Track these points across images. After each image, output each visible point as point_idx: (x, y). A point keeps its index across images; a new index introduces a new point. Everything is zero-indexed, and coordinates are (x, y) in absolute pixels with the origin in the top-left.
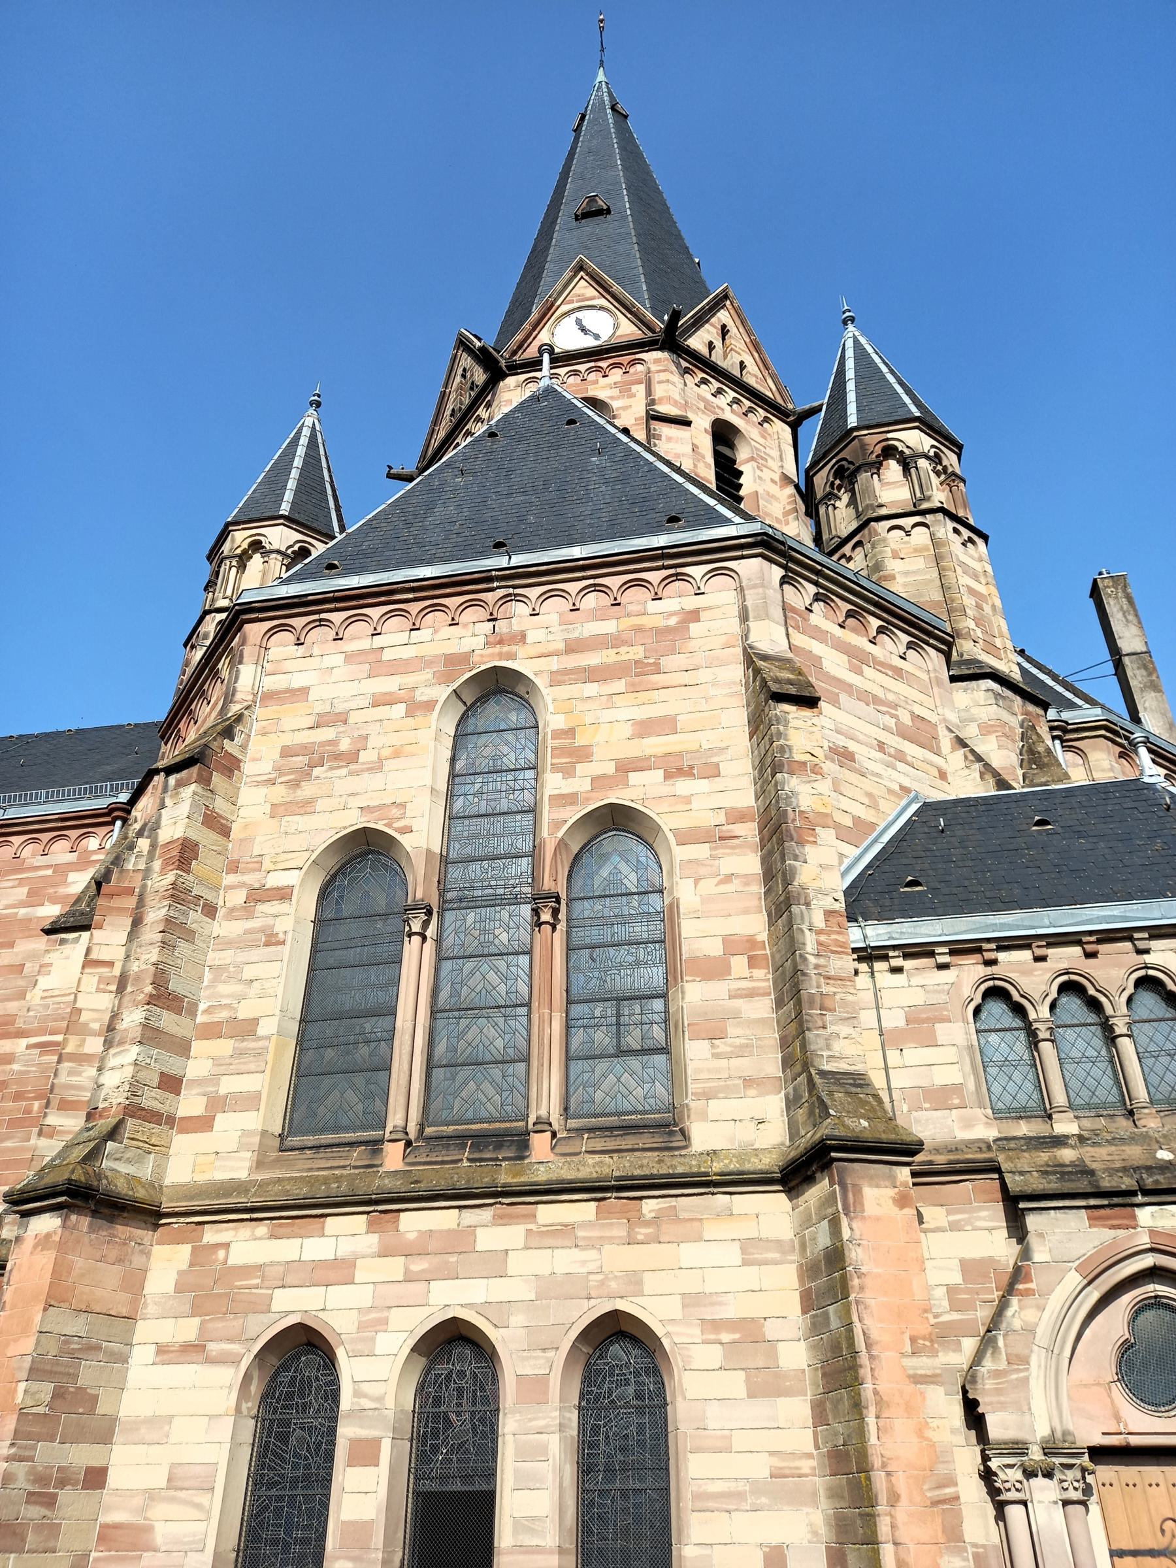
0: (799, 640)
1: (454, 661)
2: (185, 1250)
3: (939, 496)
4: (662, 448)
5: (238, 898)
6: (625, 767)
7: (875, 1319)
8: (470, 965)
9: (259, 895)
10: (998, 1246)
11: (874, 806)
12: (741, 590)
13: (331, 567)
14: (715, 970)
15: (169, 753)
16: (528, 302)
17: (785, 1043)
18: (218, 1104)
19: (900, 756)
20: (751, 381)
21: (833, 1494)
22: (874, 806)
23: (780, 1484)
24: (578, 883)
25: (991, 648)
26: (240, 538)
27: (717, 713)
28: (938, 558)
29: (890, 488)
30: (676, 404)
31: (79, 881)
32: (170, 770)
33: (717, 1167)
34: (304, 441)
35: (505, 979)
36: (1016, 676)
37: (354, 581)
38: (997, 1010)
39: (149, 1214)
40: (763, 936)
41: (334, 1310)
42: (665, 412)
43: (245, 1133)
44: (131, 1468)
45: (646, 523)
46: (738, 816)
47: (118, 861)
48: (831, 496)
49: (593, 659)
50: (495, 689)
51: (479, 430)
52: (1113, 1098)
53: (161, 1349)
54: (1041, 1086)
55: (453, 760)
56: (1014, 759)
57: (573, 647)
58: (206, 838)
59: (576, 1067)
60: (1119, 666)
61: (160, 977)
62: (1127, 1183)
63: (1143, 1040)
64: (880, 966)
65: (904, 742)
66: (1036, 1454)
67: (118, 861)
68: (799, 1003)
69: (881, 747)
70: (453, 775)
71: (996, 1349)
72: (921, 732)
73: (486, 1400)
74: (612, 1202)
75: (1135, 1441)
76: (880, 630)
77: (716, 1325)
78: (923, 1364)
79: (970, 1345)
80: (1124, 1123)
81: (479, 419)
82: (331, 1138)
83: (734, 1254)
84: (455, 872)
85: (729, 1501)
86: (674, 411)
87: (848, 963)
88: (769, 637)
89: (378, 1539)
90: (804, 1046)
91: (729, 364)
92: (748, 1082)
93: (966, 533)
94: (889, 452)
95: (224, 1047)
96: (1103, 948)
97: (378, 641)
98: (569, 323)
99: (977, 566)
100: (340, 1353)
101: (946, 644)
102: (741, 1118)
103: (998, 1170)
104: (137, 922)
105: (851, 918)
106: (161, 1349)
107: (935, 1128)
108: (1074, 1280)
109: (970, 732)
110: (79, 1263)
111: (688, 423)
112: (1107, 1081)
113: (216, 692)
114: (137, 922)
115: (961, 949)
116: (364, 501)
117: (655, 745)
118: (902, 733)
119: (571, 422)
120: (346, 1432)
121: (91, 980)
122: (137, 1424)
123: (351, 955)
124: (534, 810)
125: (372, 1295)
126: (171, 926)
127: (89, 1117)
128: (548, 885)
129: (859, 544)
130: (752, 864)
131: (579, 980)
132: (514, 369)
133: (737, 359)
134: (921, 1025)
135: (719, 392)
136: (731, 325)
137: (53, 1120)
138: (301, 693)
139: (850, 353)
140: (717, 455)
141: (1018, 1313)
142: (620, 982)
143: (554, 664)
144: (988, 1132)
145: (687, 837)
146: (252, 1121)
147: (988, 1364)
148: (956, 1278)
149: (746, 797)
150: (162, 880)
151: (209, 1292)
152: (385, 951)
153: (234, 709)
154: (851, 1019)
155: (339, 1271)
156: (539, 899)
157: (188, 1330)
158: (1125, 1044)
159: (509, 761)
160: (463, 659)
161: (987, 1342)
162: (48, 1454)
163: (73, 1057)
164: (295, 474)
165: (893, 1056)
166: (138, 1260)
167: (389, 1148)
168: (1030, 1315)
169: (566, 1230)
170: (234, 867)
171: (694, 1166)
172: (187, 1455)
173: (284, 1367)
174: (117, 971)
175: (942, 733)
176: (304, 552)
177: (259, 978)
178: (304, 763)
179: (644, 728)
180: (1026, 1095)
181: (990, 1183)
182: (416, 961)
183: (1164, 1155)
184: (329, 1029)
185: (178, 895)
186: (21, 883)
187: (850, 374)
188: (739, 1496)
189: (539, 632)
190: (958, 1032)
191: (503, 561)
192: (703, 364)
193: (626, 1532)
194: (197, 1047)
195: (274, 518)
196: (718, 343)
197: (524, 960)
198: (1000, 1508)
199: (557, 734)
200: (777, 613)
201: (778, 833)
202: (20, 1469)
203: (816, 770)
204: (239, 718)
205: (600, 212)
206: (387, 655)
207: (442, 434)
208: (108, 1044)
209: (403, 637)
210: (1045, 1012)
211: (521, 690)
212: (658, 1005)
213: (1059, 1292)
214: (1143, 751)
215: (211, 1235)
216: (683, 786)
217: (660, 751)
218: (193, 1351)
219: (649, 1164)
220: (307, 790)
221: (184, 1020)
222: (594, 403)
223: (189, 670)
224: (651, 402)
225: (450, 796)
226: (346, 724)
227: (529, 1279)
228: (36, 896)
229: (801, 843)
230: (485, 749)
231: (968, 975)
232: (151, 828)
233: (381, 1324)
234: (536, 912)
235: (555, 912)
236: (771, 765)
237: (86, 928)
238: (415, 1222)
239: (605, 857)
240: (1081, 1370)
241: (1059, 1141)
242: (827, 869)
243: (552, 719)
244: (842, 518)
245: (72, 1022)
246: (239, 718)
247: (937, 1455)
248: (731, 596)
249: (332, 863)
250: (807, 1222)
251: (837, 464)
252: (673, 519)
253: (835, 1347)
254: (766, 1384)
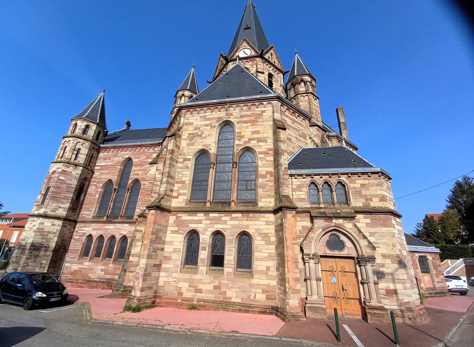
0: (283, 117)
1: (220, 118)
2: (175, 217)
3: (311, 90)
4: (259, 78)
5: (181, 160)
6: (250, 140)
7: (288, 234)
8: (221, 174)
9: (185, 160)
10: (309, 224)
11: (294, 149)
12: (273, 107)
13: (197, 99)
14: (264, 177)
15: (169, 134)
16: (234, 47)
17: (275, 190)
18: (179, 194)
19: (300, 140)
20: (276, 65)
21: (278, 259)
22: (294, 149)
23: (269, 257)
24: (240, 160)
25: (317, 120)
26: (180, 93)
27: (267, 130)
28: (309, 102)
29: (302, 88)
30: (262, 69)
31: (155, 156)
32: (169, 137)
33: (262, 209)
34: (191, 74)
35: (227, 176)
36: (321, 126)
37: (201, 102)
38: (313, 186)
39: (169, 211)
40: (273, 171)
41: (199, 227)
42: (259, 70)
43: (184, 199)
44: (168, 248)
45: (254, 93)
46: (270, 150)
47: (161, 152)
48: (290, 89)
49: (245, 119)
50: (227, 124)
51: (224, 73)
52: (331, 201)
53: (172, 231)
54: (319, 199)
55: (219, 137)
56: (320, 141)
57: (241, 117)
58: (176, 149)
59: (239, 192)
60: (339, 125)
61: (169, 173)
62: (332, 215)
63: (337, 192)
64: (293, 177)
65: (301, 137)
66: (311, 256)
67: (161, 152)
68: (279, 184)
69: (296, 138)
70: (219, 140)
71: (306, 240)
72: (304, 136)
73: (223, 242)
74: (245, 214)
75: (327, 255)
76: (298, 116)
77: (261, 234)
78: (295, 242)
79: (302, 239)
80: (332, 206)
81: (224, 71)
82: (198, 201)
83: (264, 223)
84: (219, 157)
85: (261, 259)
86: (261, 71)
87: (288, 176)
88: (277, 116)
89: (206, 261)
90: (279, 191)
91: (272, 61)
92: (269, 196)
93: (315, 98)
94: (302, 81)
95: (180, 185)
96: (332, 176)
97: (206, 114)
98: (242, 51)
99: (316, 104)
100: (200, 234)
101: (310, 120)
102: (267, 202)
103: (310, 212)
104: (165, 163)
105: (289, 169)
106: (172, 231)
107: (299, 205)
108: (321, 230)
109: (312, 136)
110: (158, 218)
111: (264, 73)
112: (330, 199)
113: (177, 123)
114: (165, 163)
115: (308, 175)
116: (203, 88)
117: (255, 136)
118: (300, 135)
119: (242, 72)
120: (201, 245)
121: (157, 173)
122: (168, 242)
123: (201, 171)
124: (233, 147)
125: (205, 226)
126: (170, 164)
127: (159, 195)
128: (235, 160)
129: (295, 99)
130: (271, 158)
131: (240, 177)
132: (231, 61)
133: (274, 60)
134: (299, 188)
135: (270, 67)
136: (273, 53)
137: (152, 195)
138: (192, 124)
139: (296, 60)
140: (269, 80)
141: (311, 235)
142: (247, 178)
143: (238, 120)
144: (308, 206)
145: (260, 153)
146: (185, 197)
147: (305, 242)
148: (301, 229)
149: (271, 146)
150: (169, 156)
151: (179, 223)
152: (207, 171)
153: (180, 126)
154: (287, 186)
155: (200, 222)
156: (233, 163)
157: (176, 229)
158: (334, 193)
159: (229, 137)
160: (220, 118)
161: (305, 239)
162: (155, 245)
163: (155, 185)
164: (190, 81)
165: (294, 193)
166: (167, 218)
167: (207, 203)
168: (313, 235)
169: (237, 218)
170: (180, 155)
171: (258, 209)
172: (175, 247)
173: (191, 235)
174: (162, 171)
175: (307, 136)
176: (192, 97)
177: (186, 174)
178: (192, 137)
179: (254, 133)
180: (315, 199)
181: (309, 214)
182: (212, 172)
183: (338, 211)
184: (197, 183)
185: (171, 159)
186: (145, 155)
187: (296, 64)
188: (263, 259)
189: (235, 113)
190: (306, 189)
191: (229, 100)
192: (267, 61)
193: (244, 262)
194: (175, 185)
195: (186, 90)
196: (270, 57)
197: (231, 173)
198: (304, 263)
199: (238, 133)
200: (279, 111)
201: (277, 153)
202: (151, 247)
203: (285, 142)
204: (181, 128)
205: (249, 28)
206: (207, 117)
207: (217, 74)
208: (161, 184)
209: (210, 113)
210: (321, 187)
211: (231, 124)
212: (254, 182)
213: (318, 232)
214: (343, 141)
215: (179, 215)
216: (260, 144)
217: (256, 137)
218: (176, 232)
219: (251, 208)
220: (193, 141)
221: (173, 180)
222: (246, 68)
223: (172, 118)
224: (257, 69)
225: (218, 143)
226: (200, 129)
227: (230, 225)
228: (147, 158)
229: (281, 155)
230: (225, 135)
231: (309, 180)
232: (166, 147)
233: (207, 230)
234: (233, 165)
235: (236, 165)
236: (277, 140)
237: (156, 164)
238: (211, 215)
239: (245, 156)
240: (320, 244)
241: (321, 208)
242: (285, 160)
243: (237, 130)
244: (292, 94)
245: (155, 179)
246: (181, 128)
247: (296, 255)
248: (271, 108)
249: (198, 154)
250: (277, 219)
251: (292, 83)
252: (261, 92)
253: (280, 238)
254: (268, 243)
